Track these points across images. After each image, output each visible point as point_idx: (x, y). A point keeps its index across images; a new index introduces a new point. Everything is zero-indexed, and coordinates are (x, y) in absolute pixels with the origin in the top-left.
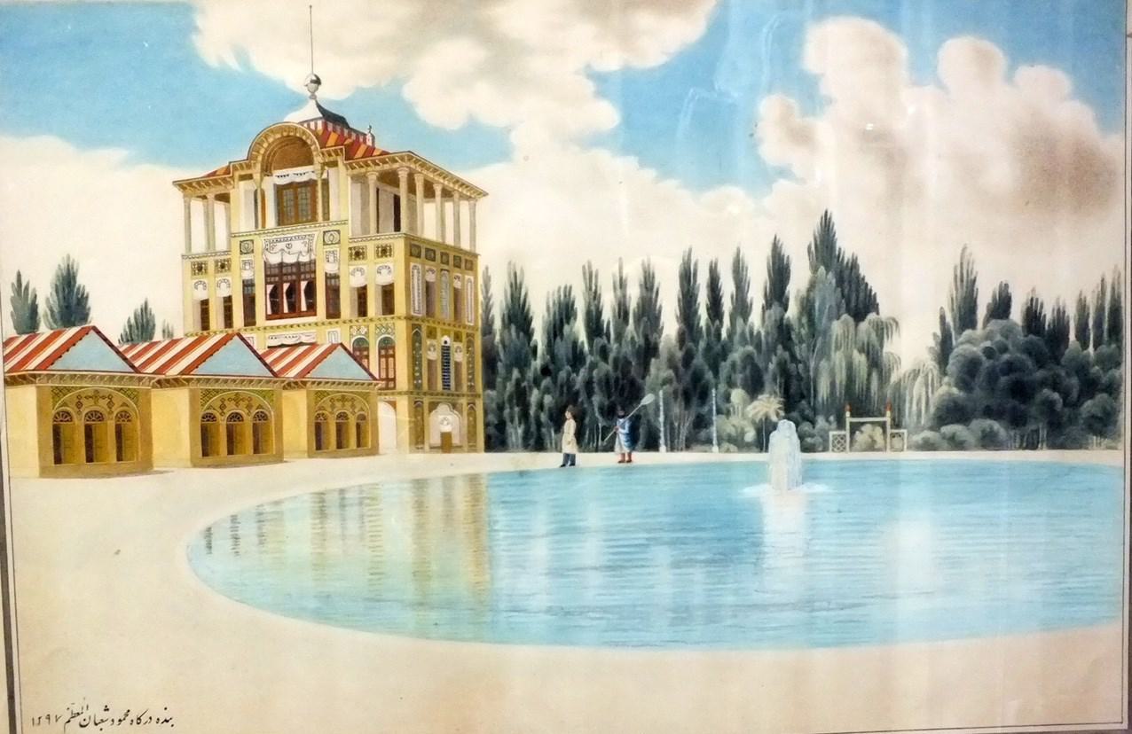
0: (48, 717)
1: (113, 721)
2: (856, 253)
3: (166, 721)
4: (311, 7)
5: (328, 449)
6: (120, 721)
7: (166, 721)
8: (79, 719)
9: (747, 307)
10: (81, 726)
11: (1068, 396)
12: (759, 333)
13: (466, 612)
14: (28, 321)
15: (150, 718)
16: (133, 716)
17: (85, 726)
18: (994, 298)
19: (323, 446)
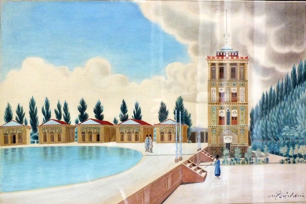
0: (272, 196)
1: (288, 196)
2: (137, 101)
3: (303, 196)
4: (226, 10)
5: (97, 135)
6: (290, 196)
7: (303, 196)
8: (280, 196)
9: (11, 120)
10: (280, 197)
11: (275, 121)
12: (258, 106)
13: (17, 158)
14: (9, 118)
15: (299, 195)
16: (294, 195)
17: (281, 197)
18: (160, 108)
19: (12, 137)
